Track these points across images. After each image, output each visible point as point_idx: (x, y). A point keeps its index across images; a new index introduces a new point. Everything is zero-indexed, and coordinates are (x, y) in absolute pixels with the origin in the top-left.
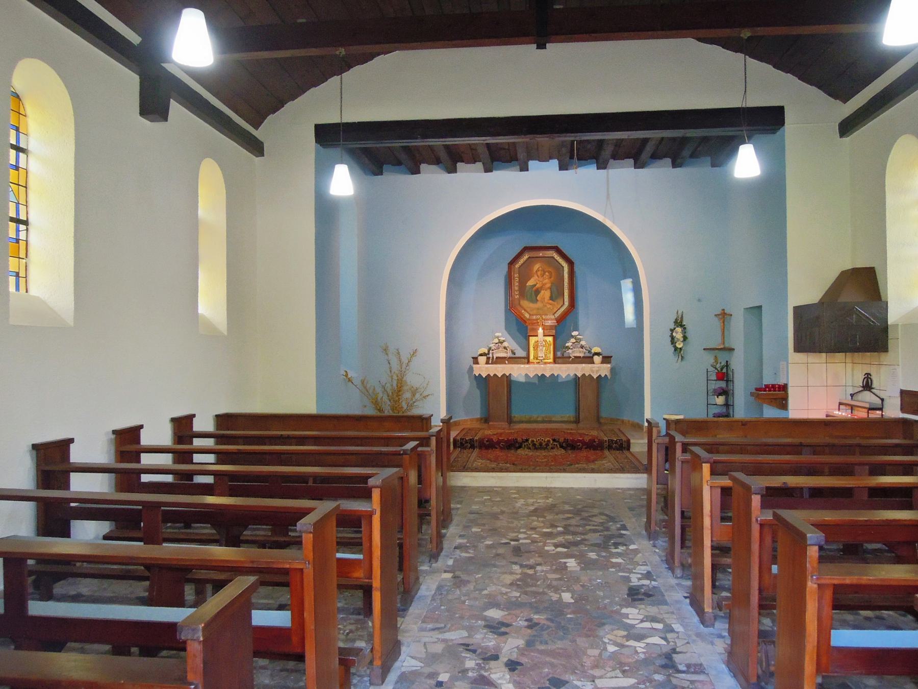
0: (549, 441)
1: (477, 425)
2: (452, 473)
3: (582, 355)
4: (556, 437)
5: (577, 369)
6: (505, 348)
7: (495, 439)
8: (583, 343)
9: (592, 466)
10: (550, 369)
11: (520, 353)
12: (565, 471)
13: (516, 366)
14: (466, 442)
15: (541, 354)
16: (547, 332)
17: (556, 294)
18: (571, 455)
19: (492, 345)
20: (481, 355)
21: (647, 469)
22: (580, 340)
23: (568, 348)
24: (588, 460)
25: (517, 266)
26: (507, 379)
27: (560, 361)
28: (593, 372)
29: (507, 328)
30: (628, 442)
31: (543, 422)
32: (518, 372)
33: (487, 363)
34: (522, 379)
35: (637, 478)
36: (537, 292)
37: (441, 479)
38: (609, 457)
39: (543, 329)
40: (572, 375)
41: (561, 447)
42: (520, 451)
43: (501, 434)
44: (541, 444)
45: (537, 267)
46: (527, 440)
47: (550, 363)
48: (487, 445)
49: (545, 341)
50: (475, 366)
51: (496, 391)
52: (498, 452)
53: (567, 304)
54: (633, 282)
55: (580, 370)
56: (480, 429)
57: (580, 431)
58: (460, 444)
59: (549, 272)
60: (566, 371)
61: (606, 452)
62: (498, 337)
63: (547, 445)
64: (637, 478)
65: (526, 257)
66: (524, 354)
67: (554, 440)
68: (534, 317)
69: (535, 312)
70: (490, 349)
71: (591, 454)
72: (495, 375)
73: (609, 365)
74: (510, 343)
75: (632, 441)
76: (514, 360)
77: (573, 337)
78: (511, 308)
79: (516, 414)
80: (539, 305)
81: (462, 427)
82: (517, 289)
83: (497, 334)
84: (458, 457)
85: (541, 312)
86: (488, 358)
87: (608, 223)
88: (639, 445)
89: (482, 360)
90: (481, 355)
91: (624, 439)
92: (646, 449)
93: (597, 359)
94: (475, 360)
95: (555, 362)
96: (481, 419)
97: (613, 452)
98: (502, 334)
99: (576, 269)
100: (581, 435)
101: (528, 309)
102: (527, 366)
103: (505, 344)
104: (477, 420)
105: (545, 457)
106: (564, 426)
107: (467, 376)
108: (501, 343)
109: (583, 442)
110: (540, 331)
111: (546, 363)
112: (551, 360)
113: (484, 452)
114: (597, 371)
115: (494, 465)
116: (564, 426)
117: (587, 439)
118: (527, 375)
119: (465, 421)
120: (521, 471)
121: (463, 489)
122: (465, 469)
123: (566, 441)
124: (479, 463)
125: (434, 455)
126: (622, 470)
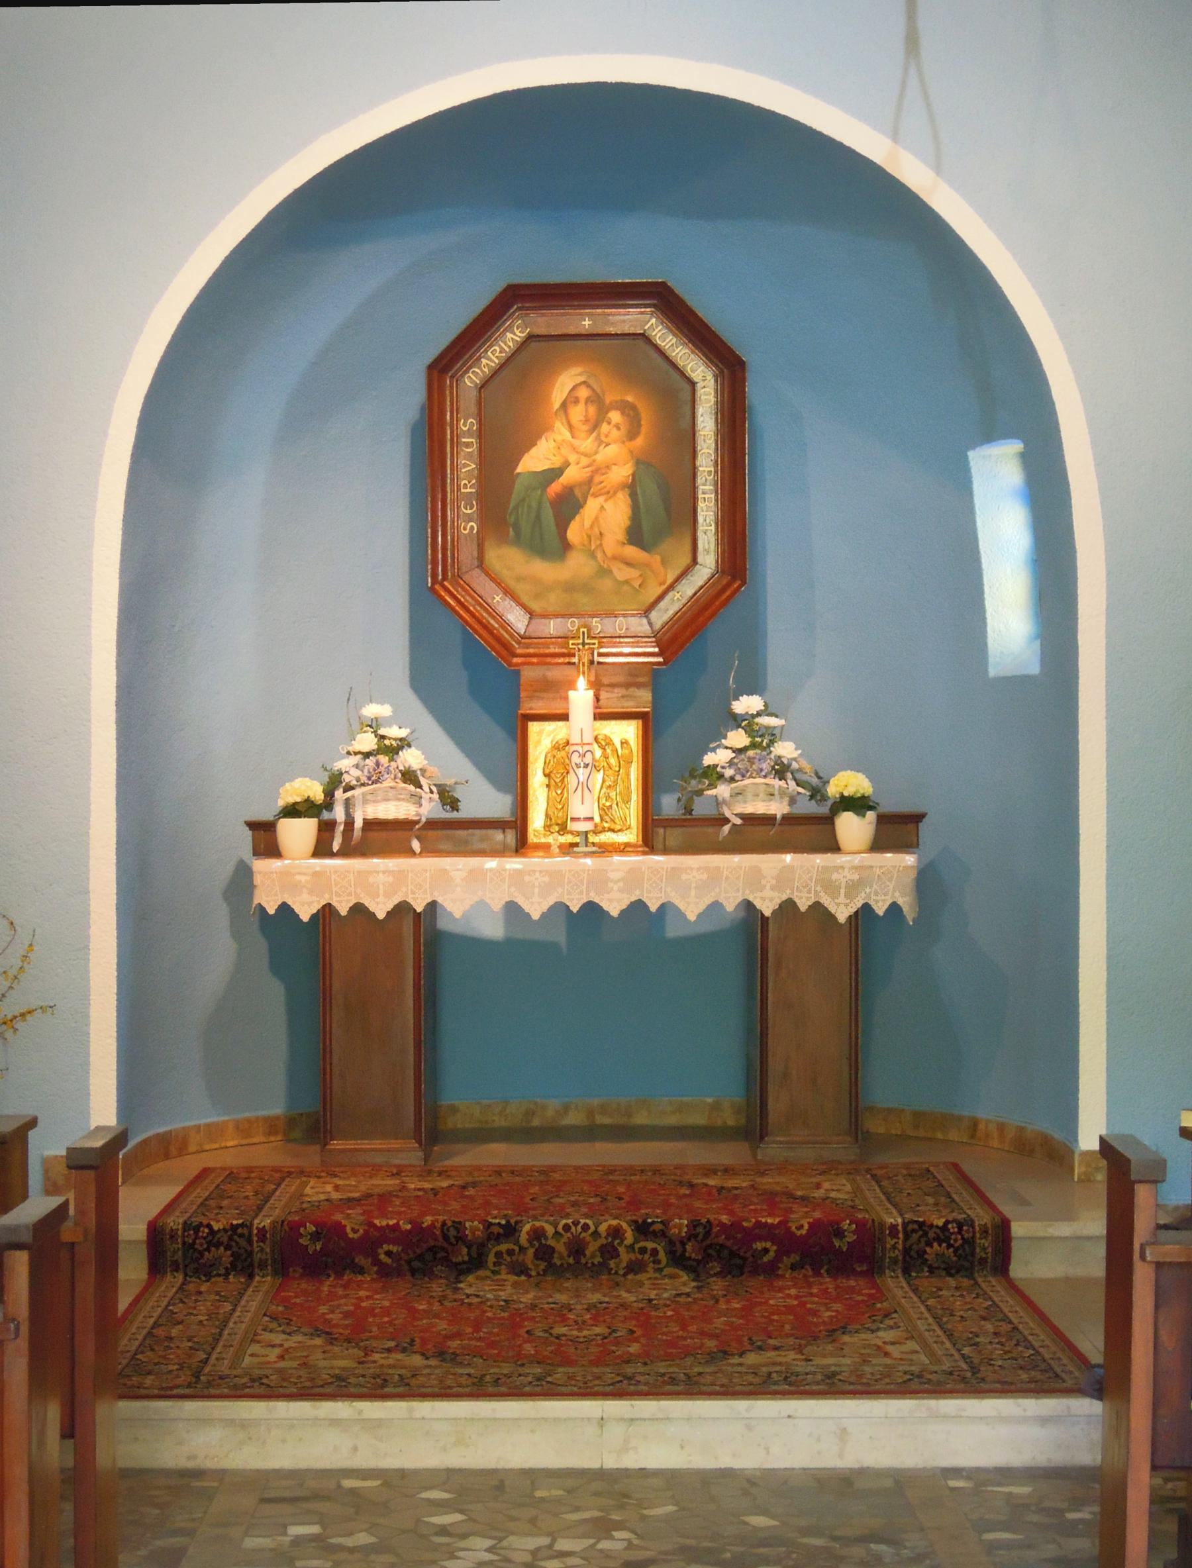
0: (616, 1233)
1: (268, 1154)
2: (126, 1407)
3: (778, 808)
4: (654, 1216)
5: (755, 877)
6: (409, 776)
7: (352, 1223)
8: (785, 750)
9: (825, 1359)
10: (627, 879)
11: (484, 799)
12: (691, 1388)
13: (457, 866)
14: (213, 1238)
15: (583, 806)
16: (612, 701)
17: (660, 515)
18: (725, 1301)
19: (345, 764)
20: (292, 811)
21: (1108, 1382)
22: (773, 736)
23: (713, 775)
24: (808, 1333)
25: (472, 378)
26: (420, 928)
27: (674, 836)
28: (831, 888)
29: (423, 681)
30: (1004, 1227)
31: (590, 1133)
32: (470, 891)
33: (322, 849)
34: (493, 929)
35: (1044, 1421)
36: (568, 505)
37: (56, 1452)
38: (911, 1312)
39: (596, 686)
40: (730, 905)
41: (678, 1260)
42: (470, 1285)
43: (384, 1199)
44: (577, 1249)
45: (566, 382)
46: (510, 1231)
47: (623, 849)
48: (312, 1255)
49: (604, 743)
50: (263, 867)
51: (362, 998)
52: (365, 1294)
53: (708, 561)
54: (1026, 459)
55: (770, 880)
56: (284, 1175)
57: (768, 1182)
58: (182, 1251)
59: (628, 409)
60: (701, 887)
61: (895, 1285)
62: (373, 725)
63: (609, 1251)
64: (1044, 1421)
65: (512, 336)
66: (497, 805)
67: (642, 1229)
68: (552, 627)
69: (553, 601)
70: (334, 782)
71: (822, 1296)
72: (359, 909)
73: (910, 860)
74: (432, 753)
75: (1018, 1229)
76: (449, 831)
77: (736, 721)
78: (436, 578)
79: (465, 1092)
80: (576, 565)
81: (191, 1165)
82: (465, 495)
83: (372, 710)
84: (168, 1317)
85: (584, 602)
86: (327, 828)
87: (913, 172)
88: (1057, 1245)
89: (298, 834)
90: (292, 811)
91: (982, 1217)
92: (1095, 1265)
93: (853, 829)
94: (265, 838)
95: (649, 843)
96: (291, 1122)
97: (926, 1282)
98: (390, 710)
99: (755, 391)
100: (771, 1199)
101: (517, 593)
102: (514, 864)
103: (412, 758)
104: (271, 1125)
105: (597, 1313)
106: (696, 1154)
107: (221, 915)
108: (393, 750)
109: (786, 1241)
110: (581, 698)
111: (605, 850)
112: (631, 836)
113: (300, 1288)
114: (853, 888)
115: (343, 1360)
116: (696, 1154)
117: (801, 1222)
118: (512, 909)
119: (214, 1131)
120: (479, 1390)
121: (190, 1483)
122: (202, 1383)
123: (700, 1230)
124: (267, 1351)
125: (23, 1343)
126: (970, 1381)
